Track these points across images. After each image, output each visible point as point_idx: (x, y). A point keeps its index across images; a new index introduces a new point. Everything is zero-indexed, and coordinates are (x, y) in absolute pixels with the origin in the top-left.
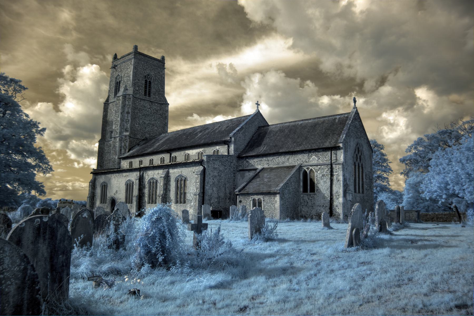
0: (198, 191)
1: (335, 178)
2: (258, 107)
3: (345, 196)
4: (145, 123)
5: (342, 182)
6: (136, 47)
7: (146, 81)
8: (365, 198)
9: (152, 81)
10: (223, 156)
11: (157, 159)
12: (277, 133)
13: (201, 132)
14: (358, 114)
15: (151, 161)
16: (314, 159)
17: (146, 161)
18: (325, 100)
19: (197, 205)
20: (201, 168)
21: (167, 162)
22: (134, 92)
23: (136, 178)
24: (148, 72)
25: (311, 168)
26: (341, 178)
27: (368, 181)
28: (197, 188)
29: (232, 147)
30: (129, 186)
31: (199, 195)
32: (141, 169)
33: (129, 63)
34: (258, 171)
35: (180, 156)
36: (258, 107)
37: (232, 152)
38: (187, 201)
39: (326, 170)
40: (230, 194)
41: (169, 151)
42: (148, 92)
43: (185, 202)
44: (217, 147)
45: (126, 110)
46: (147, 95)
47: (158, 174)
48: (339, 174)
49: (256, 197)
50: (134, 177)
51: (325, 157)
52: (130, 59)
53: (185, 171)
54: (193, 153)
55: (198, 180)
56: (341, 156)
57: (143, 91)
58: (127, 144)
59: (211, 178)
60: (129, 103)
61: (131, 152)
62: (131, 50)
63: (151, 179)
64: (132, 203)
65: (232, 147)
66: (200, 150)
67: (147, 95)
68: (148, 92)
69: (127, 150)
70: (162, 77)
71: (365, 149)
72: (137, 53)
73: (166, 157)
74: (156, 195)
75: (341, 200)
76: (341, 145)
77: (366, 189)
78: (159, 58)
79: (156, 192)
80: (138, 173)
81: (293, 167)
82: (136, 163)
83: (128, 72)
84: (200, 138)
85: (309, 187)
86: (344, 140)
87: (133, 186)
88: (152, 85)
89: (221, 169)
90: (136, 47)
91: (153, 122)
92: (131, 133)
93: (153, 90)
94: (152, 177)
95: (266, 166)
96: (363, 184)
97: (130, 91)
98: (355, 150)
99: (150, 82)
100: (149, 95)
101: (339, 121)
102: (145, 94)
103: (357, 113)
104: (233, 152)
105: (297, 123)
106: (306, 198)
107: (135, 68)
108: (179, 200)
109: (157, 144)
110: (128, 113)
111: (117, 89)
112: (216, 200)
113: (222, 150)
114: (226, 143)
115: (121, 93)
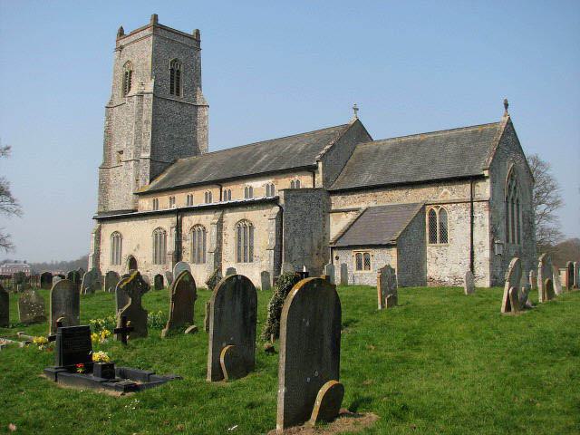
0: (273, 243)
3: (492, 249)
4: (173, 138)
5: (488, 228)
6: (155, 18)
7: (172, 70)
9: (182, 69)
10: (307, 190)
11: (199, 198)
12: (387, 153)
13: (266, 151)
14: (511, 124)
15: (172, 200)
16: (446, 193)
17: (181, 200)
18: (278, 427)
19: (272, 264)
20: (276, 209)
21: (215, 201)
22: (155, 88)
23: (171, 225)
24: (175, 55)
25: (441, 206)
26: (487, 222)
28: (271, 239)
29: (319, 177)
30: (159, 237)
31: (274, 249)
32: (180, 212)
33: (145, 41)
34: (361, 211)
35: (237, 193)
37: (319, 184)
38: (255, 259)
39: (464, 211)
40: (319, 247)
41: (219, 183)
42: (175, 89)
43: (251, 261)
44: (297, 177)
45: (144, 118)
47: (208, 220)
48: (483, 217)
49: (362, 251)
50: (167, 223)
51: (463, 191)
52: (146, 37)
53: (253, 215)
54: (259, 188)
55: (273, 227)
56: (484, 190)
58: (148, 172)
59: (292, 224)
60: (148, 105)
61: (154, 183)
62: (148, 21)
63: (195, 226)
64: (165, 263)
65: (319, 177)
66: (269, 181)
67: (175, 93)
68: (175, 89)
69: (148, 181)
70: (196, 63)
71: (522, 176)
72: (157, 27)
73: (215, 192)
74: (204, 250)
75: (487, 254)
76: (486, 173)
77: (524, 238)
78: (191, 32)
79: (204, 246)
80: (175, 219)
81: (415, 205)
82: (164, 203)
83: (142, 53)
84: (265, 162)
85: (438, 235)
86: (491, 165)
87: (165, 237)
88: (182, 75)
90: (155, 18)
92: (153, 153)
94: (197, 223)
95: (372, 204)
96: (507, 224)
97: (150, 87)
99: (178, 71)
102: (172, 93)
103: (510, 124)
104: (321, 184)
105: (417, 138)
107: (155, 51)
108: (242, 258)
110: (146, 122)
111: (127, 86)
113: (305, 181)
114: (312, 170)
115: (134, 90)
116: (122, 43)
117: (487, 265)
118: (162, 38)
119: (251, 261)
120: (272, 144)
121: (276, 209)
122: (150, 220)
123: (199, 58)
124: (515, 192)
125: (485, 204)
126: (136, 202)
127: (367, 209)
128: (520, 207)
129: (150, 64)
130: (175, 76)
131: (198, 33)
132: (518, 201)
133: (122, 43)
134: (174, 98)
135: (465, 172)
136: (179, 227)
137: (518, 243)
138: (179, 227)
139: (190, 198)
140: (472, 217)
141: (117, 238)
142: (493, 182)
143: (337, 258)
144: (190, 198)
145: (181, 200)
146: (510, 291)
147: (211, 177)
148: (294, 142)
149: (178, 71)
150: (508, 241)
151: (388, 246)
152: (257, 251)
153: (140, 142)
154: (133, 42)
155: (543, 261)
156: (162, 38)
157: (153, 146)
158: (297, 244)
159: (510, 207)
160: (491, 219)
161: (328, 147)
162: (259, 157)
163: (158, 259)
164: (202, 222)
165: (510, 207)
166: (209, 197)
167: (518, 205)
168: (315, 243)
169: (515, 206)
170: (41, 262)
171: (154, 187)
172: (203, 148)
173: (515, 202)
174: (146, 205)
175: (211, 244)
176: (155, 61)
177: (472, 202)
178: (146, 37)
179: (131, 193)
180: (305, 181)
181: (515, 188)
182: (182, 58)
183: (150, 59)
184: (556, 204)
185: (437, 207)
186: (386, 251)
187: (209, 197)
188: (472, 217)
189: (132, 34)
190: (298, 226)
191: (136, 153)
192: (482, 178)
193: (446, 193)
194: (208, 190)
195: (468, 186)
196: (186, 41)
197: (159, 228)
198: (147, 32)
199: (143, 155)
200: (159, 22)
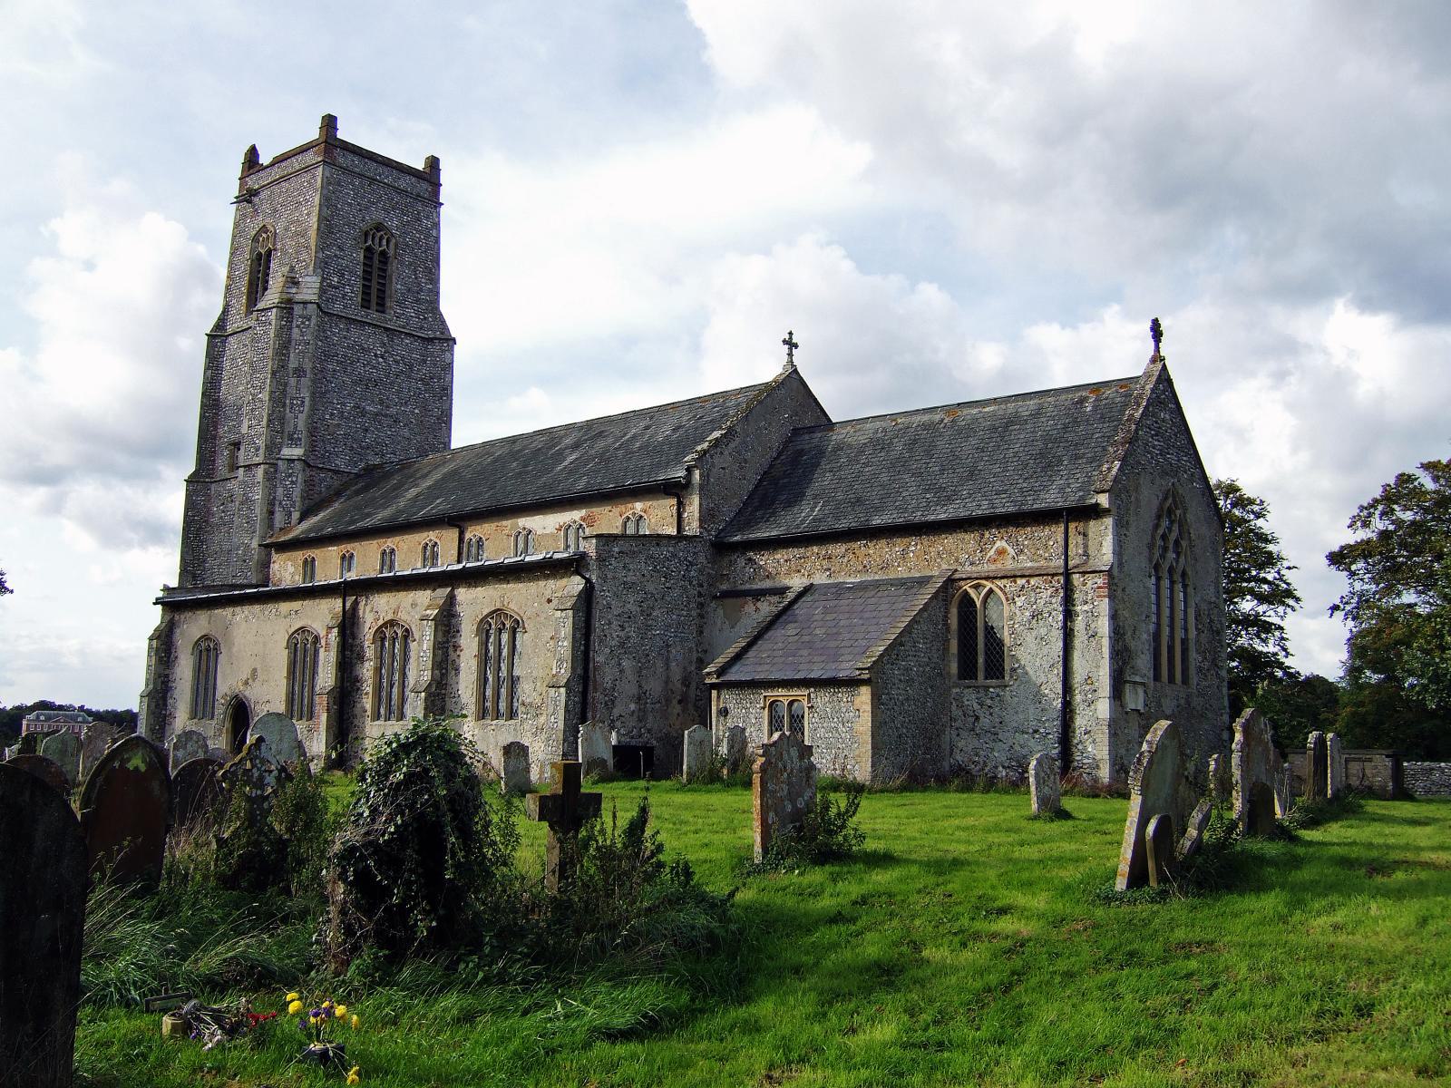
0: (565, 673)
1: (1079, 624)
2: (790, 355)
4: (363, 413)
5: (1106, 642)
6: (330, 123)
8: (1196, 702)
10: (658, 539)
13: (576, 446)
14: (1169, 382)
15: (347, 560)
16: (1003, 550)
17: (367, 560)
20: (575, 584)
21: (447, 562)
23: (328, 620)
24: (376, 215)
25: (989, 585)
26: (1104, 626)
27: (1204, 637)
30: (302, 651)
31: (567, 686)
34: (790, 596)
36: (790, 355)
37: (692, 528)
39: (1048, 597)
41: (457, 521)
46: (374, 305)
47: (416, 608)
48: (1096, 615)
50: (321, 616)
51: (1044, 546)
52: (307, 169)
53: (516, 596)
54: (548, 531)
55: (566, 630)
56: (1102, 542)
57: (358, 288)
61: (305, 525)
62: (313, 133)
63: (385, 625)
65: (693, 507)
67: (374, 305)
70: (428, 236)
73: (446, 541)
74: (403, 686)
75: (1103, 708)
76: (1103, 500)
78: (419, 165)
79: (404, 675)
82: (329, 566)
83: (300, 215)
85: (981, 660)
88: (394, 266)
89: (650, 587)
90: (330, 123)
91: (393, 411)
93: (397, 286)
94: (389, 617)
95: (820, 579)
97: (309, 289)
98: (1159, 517)
99: (383, 253)
100: (382, 308)
101: (1095, 408)
102: (366, 304)
103: (1165, 380)
104: (696, 524)
106: (970, 698)
107: (327, 202)
109: (413, 492)
110: (299, 372)
111: (257, 285)
112: (633, 706)
113: (657, 516)
114: (676, 490)
116: (253, 183)
117: (1103, 737)
118: (345, 170)
119: (512, 714)
120: (593, 430)
121: (575, 584)
122: (317, 601)
123: (437, 225)
124: (1178, 554)
125: (1100, 581)
126: (265, 565)
127: (808, 590)
128: (1190, 590)
129: (313, 233)
130: (376, 267)
131: (433, 163)
132: (1184, 574)
133: (253, 183)
134: (374, 316)
135: (1051, 498)
136: (447, 621)
137: (1185, 681)
138: (447, 621)
139: (388, 557)
140: (1069, 615)
141: (208, 652)
142: (1120, 527)
143: (724, 712)
144: (388, 557)
145: (367, 560)
146: (1151, 829)
147: (439, 506)
148: (642, 424)
149: (383, 253)
150: (1157, 677)
151: (852, 683)
152: (527, 692)
153: (282, 420)
154: (277, 182)
155: (1246, 729)
156: (345, 170)
157: (313, 431)
158: (630, 674)
159: (1166, 593)
160: (1114, 617)
161: (717, 434)
162: (560, 456)
163: (200, 708)
164: (403, 616)
165: (1166, 593)
166: (430, 553)
167: (1185, 586)
168: (676, 673)
169: (1179, 587)
170: (120, 708)
171: (309, 530)
172: (447, 444)
173: (1177, 577)
174: (286, 571)
175: (420, 670)
176: (327, 227)
177: (1067, 574)
178: (307, 169)
179: (255, 544)
180: (657, 516)
181: (1177, 543)
182: (393, 223)
183: (314, 220)
184: (461, 651)
185: (976, 587)
186: (843, 695)
187: (430, 553)
188: (1069, 615)
189: (279, 160)
190: (631, 631)
191: (272, 448)
192: (1095, 512)
193: (1001, 552)
194: (432, 535)
195: (1059, 530)
196: (405, 182)
197: (302, 630)
198: (311, 157)
199: (288, 452)
200: (340, 135)
